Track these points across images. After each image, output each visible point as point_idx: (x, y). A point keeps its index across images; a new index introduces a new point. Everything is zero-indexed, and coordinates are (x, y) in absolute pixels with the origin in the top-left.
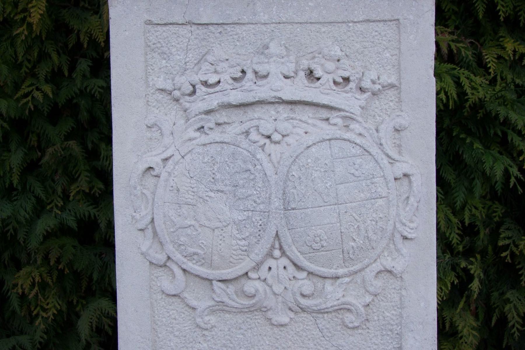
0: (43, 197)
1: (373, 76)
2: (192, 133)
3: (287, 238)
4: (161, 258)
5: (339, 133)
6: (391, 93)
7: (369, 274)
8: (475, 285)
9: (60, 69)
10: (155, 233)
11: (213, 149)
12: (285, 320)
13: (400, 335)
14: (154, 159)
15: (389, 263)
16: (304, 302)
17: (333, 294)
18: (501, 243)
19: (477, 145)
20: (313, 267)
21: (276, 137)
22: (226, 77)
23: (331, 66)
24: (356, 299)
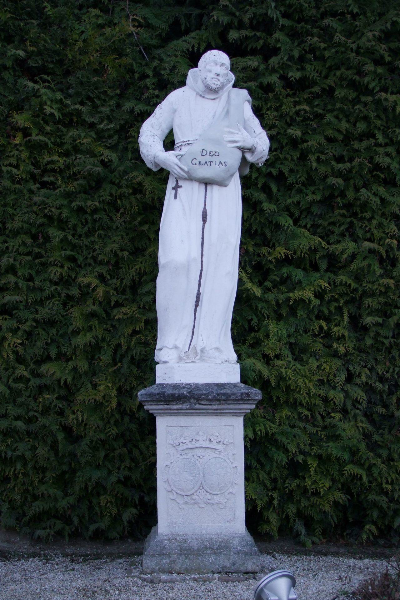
0: (111, 468)
1: (227, 440)
2: (179, 456)
3: (204, 484)
4: (170, 489)
5: (218, 456)
6: (232, 445)
7: (226, 494)
8: (276, 502)
9: (118, 421)
10: (169, 483)
11: (184, 460)
12: (204, 506)
13: (235, 511)
14: (168, 463)
15: (231, 490)
16: (208, 501)
17: (216, 499)
18: (285, 486)
19: (274, 449)
20: (211, 492)
21: (201, 457)
22: (188, 441)
23: (215, 438)
24: (223, 500)
